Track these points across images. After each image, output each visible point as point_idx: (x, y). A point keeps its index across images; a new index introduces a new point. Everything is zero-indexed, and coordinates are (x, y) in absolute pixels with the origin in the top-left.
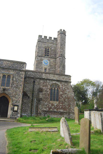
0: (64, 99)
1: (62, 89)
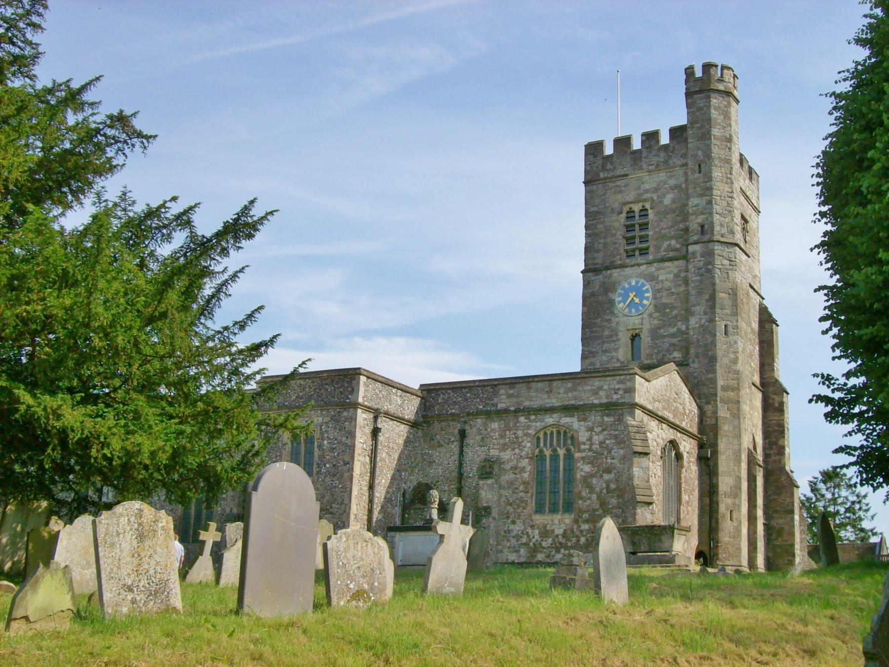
0: (598, 498)
1: (590, 450)
